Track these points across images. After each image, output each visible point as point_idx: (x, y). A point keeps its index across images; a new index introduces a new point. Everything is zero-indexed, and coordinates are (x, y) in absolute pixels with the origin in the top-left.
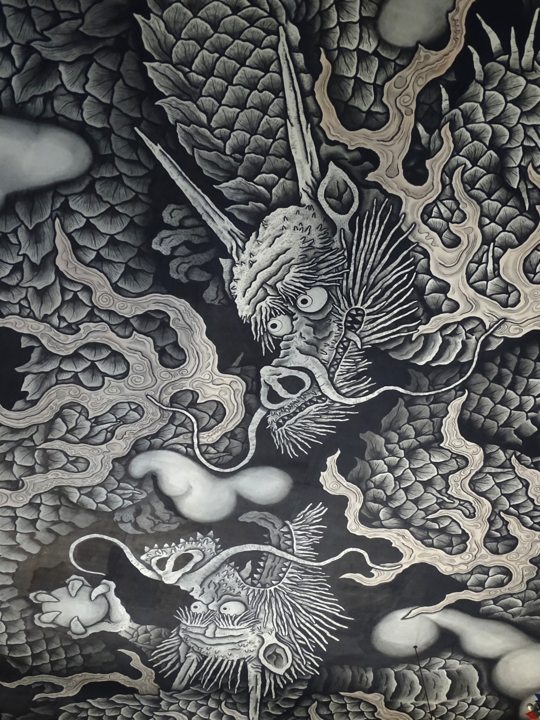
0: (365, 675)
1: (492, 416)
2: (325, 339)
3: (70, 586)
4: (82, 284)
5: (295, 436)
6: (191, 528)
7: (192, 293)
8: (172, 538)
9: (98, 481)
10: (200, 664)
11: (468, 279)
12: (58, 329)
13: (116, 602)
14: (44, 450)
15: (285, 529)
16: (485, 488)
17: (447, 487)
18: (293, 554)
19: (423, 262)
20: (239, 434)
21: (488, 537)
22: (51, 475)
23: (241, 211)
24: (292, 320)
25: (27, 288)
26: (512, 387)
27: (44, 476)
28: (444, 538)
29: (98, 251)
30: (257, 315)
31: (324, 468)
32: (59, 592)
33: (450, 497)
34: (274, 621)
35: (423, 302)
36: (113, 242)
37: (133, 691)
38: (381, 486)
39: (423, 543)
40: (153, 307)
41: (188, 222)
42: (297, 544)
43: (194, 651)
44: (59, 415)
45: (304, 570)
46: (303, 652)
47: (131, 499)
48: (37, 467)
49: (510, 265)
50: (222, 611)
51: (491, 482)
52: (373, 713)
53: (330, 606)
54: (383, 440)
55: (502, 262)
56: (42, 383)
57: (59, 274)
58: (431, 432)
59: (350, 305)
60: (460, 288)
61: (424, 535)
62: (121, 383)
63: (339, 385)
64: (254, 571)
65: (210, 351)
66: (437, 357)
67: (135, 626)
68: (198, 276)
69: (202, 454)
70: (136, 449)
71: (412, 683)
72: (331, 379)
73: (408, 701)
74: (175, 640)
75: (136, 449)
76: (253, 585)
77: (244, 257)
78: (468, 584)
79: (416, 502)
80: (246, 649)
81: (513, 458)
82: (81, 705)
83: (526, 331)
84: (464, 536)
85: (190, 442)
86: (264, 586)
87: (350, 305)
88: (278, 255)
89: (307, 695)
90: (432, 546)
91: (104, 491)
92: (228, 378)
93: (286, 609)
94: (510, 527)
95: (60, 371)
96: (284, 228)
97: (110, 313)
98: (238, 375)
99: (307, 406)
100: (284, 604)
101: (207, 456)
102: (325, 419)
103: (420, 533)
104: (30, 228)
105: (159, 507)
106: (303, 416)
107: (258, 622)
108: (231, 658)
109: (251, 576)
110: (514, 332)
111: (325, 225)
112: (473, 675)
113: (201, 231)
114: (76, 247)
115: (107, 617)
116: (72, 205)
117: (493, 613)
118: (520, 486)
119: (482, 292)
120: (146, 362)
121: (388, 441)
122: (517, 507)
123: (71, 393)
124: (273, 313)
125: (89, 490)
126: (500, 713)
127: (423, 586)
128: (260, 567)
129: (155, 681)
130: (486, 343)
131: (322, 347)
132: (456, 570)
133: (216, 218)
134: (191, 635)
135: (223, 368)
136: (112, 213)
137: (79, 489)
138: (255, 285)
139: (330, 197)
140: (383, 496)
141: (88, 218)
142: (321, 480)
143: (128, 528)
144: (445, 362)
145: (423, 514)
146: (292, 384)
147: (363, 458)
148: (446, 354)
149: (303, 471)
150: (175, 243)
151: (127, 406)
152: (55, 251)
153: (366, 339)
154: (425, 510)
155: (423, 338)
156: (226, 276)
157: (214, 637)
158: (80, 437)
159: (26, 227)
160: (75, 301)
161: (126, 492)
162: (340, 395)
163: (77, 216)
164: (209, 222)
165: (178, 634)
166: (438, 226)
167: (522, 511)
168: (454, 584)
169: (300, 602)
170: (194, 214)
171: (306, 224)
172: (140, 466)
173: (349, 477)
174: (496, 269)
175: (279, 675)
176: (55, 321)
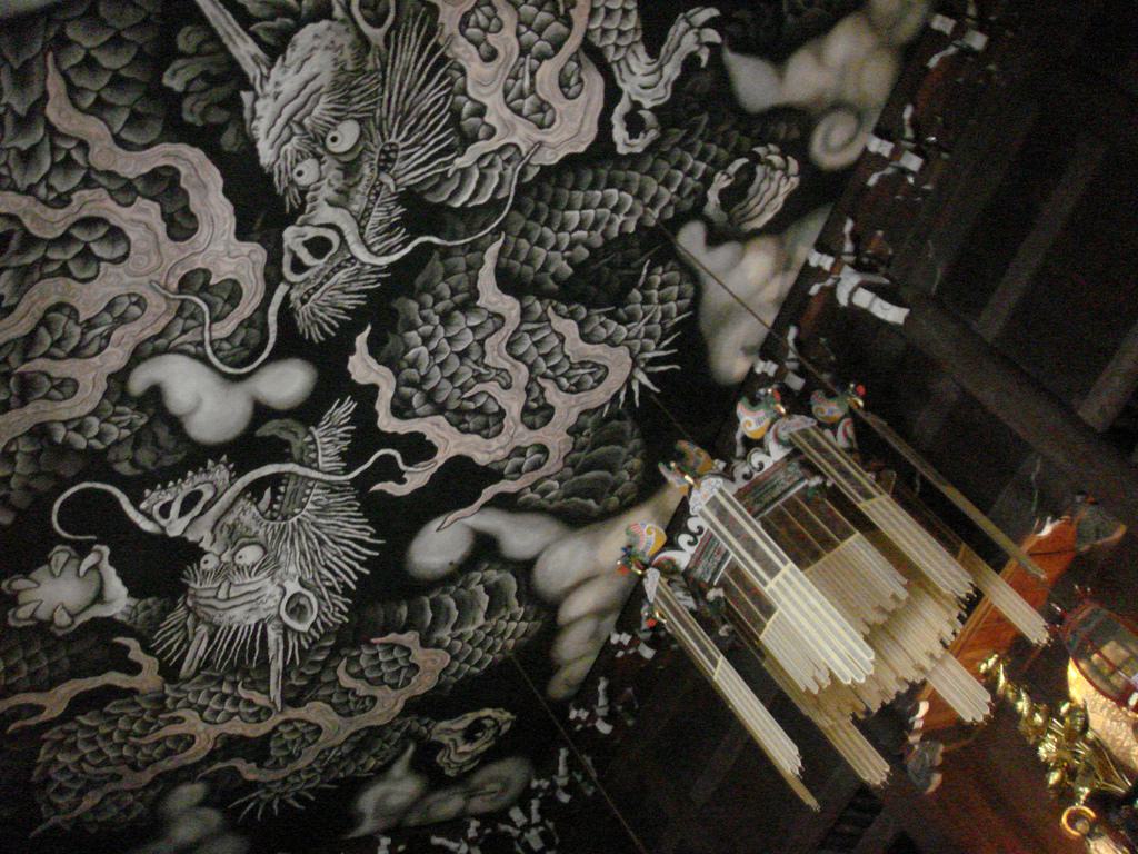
1: (529, 261)
2: (356, 184)
3: (53, 563)
4: (76, 138)
5: (321, 314)
6: (200, 456)
7: (205, 138)
8: (176, 473)
9: (90, 407)
10: (211, 638)
11: (506, 96)
12: (45, 202)
13: (110, 573)
14: (22, 375)
15: (308, 439)
16: (521, 350)
17: (484, 354)
18: (317, 469)
19: (460, 80)
20: (256, 321)
21: (526, 410)
22: (29, 409)
23: (268, 30)
24: (321, 164)
25: (8, 149)
26: (548, 223)
27: (21, 411)
28: (480, 419)
29: (98, 92)
30: (281, 161)
31: (352, 351)
32: (40, 573)
33: (486, 367)
35: (459, 130)
36: (117, 81)
37: (133, 692)
38: (414, 364)
39: (459, 429)
40: (162, 162)
41: (208, 47)
42: (324, 456)
43: (206, 623)
44: (44, 322)
45: (331, 488)
47: (129, 427)
48: (13, 400)
49: (546, 80)
50: (237, 561)
51: (528, 341)
52: (407, 658)
53: (357, 529)
55: (538, 76)
56: (23, 280)
57: (51, 130)
59: (384, 140)
60: (497, 113)
61: (459, 419)
62: (120, 269)
63: (370, 242)
64: (273, 500)
65: (227, 214)
66: (475, 194)
67: (133, 602)
68: (217, 116)
69: (215, 352)
70: (138, 357)
71: (448, 609)
72: (361, 235)
73: (444, 634)
74: (181, 612)
75: (138, 357)
76: (273, 519)
77: (269, 88)
78: (506, 472)
79: (452, 378)
80: (265, 606)
81: (550, 309)
82: (67, 727)
83: (561, 155)
84: (501, 413)
85: (199, 339)
86: (285, 518)
87: (384, 140)
88: (307, 83)
89: (335, 652)
90: (467, 431)
91: (95, 421)
92: (247, 247)
94: (547, 394)
95: (45, 260)
96: (313, 49)
97: (111, 175)
98: (258, 242)
100: (308, 538)
101: (221, 354)
102: (355, 287)
104: (16, 67)
105: (163, 433)
107: (278, 567)
108: (248, 622)
110: (550, 158)
111: (359, 42)
112: (512, 584)
113: (220, 57)
114: (73, 92)
115: (99, 598)
116: (71, 33)
118: (557, 342)
119: (518, 112)
120: (151, 238)
121: (422, 307)
122: (553, 368)
123: (59, 289)
124: (300, 157)
125: (76, 423)
126: (538, 624)
127: (460, 483)
128: (280, 493)
129: (159, 673)
130: (523, 173)
131: (352, 195)
132: (493, 457)
133: (238, 40)
134: (202, 601)
135: (242, 233)
136: (117, 42)
137: (65, 423)
138: (281, 122)
139: (365, 7)
140: (417, 377)
141: (88, 50)
142: (350, 367)
143: (124, 468)
144: (481, 200)
145: (458, 392)
146: (318, 247)
148: (483, 190)
149: (328, 358)
150: (190, 76)
151: (126, 299)
152: (45, 97)
154: (462, 388)
155: (459, 174)
156: (247, 114)
157: (228, 599)
158: (68, 350)
159: (12, 68)
160: (68, 164)
161: (123, 418)
162: (372, 258)
163: (75, 48)
164: (231, 47)
165: (185, 603)
166: (476, 38)
167: (559, 372)
168: (492, 474)
170: (213, 36)
171: (339, 41)
172: (139, 382)
173: (384, 354)
174: (532, 84)
175: (304, 633)
176: (42, 191)
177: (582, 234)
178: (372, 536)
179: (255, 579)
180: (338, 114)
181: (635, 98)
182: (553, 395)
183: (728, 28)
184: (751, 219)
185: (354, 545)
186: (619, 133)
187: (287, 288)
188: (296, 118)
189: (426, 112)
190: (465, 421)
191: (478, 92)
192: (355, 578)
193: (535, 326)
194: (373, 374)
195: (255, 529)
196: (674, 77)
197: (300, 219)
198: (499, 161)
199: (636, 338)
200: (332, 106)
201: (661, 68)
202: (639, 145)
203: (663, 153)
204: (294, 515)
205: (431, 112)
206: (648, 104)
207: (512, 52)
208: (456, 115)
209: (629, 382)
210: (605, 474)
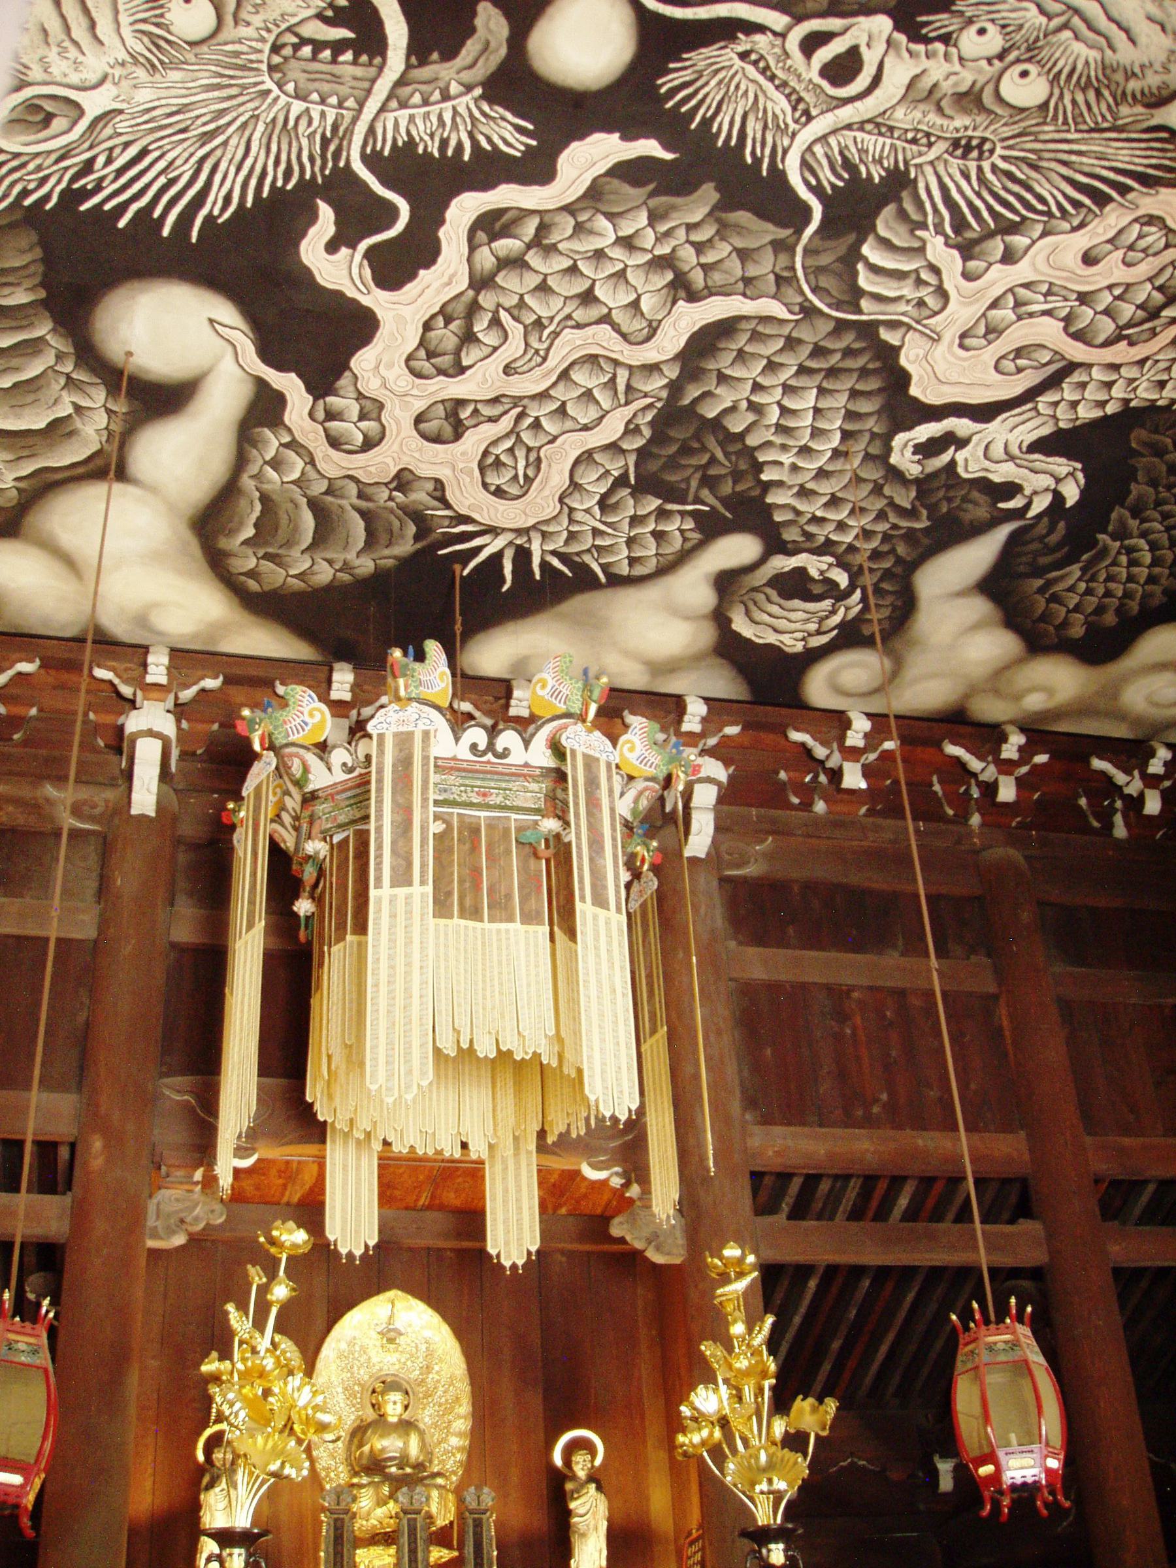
0: (21, 289)
2: (940, 110)
5: (713, 83)
15: (454, 88)
18: (383, 109)
19: (1066, 226)
21: (460, 403)
24: (989, 61)
31: (625, 138)
34: (163, 102)
46: (66, 169)
54: (696, 217)
58: (710, 284)
60: (999, 278)
63: (832, 141)
64: (318, 46)
76: (276, 49)
81: (649, 400)
88: (1127, 31)
93: (204, 119)
99: (788, 96)
100: (222, 113)
103: (460, 308)
106: (764, 92)
109: (304, 41)
111: (1165, 93)
117: (255, 447)
144: (865, 281)
147: (652, 195)
153: (928, 170)
155: (916, 244)
169: (233, 142)
174: (1031, 315)
177: (774, 415)
178: (210, 218)
179: (126, 31)
180: (1063, 77)
181: (975, 439)
182: (474, 441)
183: (1046, 519)
184: (748, 613)
185: (191, 193)
186: (925, 431)
187: (778, 28)
188: (1076, 21)
189: (1029, 189)
190: (448, 321)
191: (1042, 249)
192: (107, 207)
193: (621, 388)
194: (575, 173)
195: (257, 21)
196: (991, 476)
197: (901, 38)
198: (923, 292)
199: (571, 521)
200: (1080, 66)
201: (1011, 458)
202: (911, 467)
203: (882, 486)
204: (280, 86)
205: (1028, 196)
206: (960, 456)
207: (1088, 283)
208: (1013, 228)
209: (493, 531)
210: (307, 538)
